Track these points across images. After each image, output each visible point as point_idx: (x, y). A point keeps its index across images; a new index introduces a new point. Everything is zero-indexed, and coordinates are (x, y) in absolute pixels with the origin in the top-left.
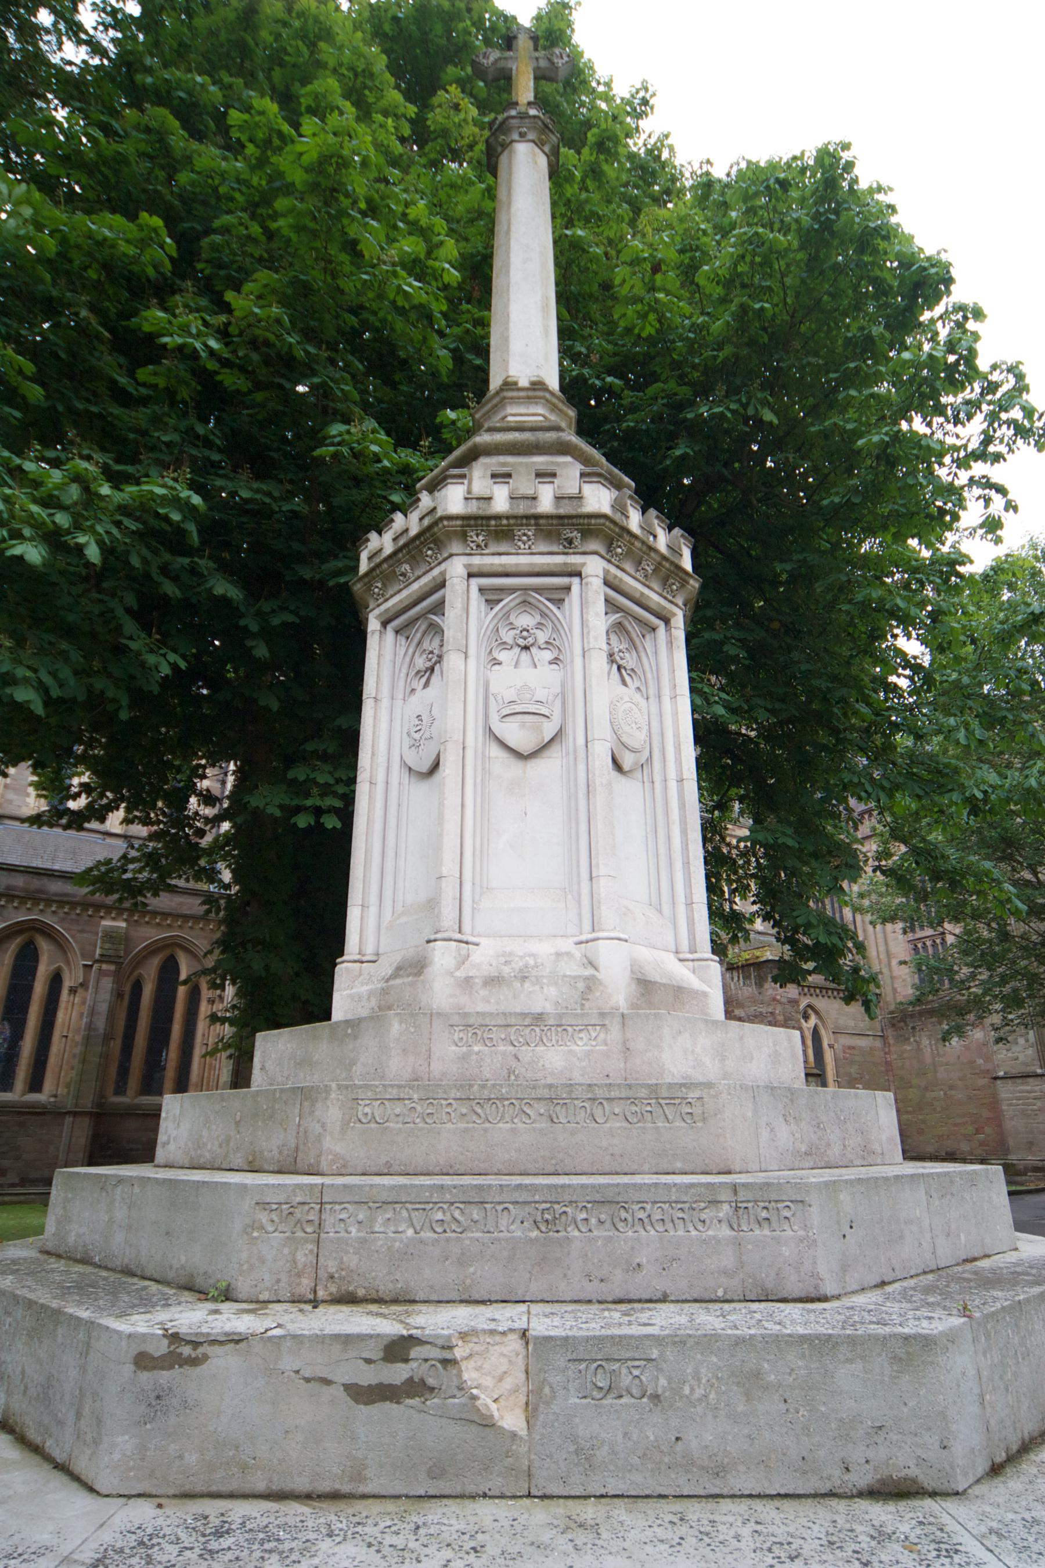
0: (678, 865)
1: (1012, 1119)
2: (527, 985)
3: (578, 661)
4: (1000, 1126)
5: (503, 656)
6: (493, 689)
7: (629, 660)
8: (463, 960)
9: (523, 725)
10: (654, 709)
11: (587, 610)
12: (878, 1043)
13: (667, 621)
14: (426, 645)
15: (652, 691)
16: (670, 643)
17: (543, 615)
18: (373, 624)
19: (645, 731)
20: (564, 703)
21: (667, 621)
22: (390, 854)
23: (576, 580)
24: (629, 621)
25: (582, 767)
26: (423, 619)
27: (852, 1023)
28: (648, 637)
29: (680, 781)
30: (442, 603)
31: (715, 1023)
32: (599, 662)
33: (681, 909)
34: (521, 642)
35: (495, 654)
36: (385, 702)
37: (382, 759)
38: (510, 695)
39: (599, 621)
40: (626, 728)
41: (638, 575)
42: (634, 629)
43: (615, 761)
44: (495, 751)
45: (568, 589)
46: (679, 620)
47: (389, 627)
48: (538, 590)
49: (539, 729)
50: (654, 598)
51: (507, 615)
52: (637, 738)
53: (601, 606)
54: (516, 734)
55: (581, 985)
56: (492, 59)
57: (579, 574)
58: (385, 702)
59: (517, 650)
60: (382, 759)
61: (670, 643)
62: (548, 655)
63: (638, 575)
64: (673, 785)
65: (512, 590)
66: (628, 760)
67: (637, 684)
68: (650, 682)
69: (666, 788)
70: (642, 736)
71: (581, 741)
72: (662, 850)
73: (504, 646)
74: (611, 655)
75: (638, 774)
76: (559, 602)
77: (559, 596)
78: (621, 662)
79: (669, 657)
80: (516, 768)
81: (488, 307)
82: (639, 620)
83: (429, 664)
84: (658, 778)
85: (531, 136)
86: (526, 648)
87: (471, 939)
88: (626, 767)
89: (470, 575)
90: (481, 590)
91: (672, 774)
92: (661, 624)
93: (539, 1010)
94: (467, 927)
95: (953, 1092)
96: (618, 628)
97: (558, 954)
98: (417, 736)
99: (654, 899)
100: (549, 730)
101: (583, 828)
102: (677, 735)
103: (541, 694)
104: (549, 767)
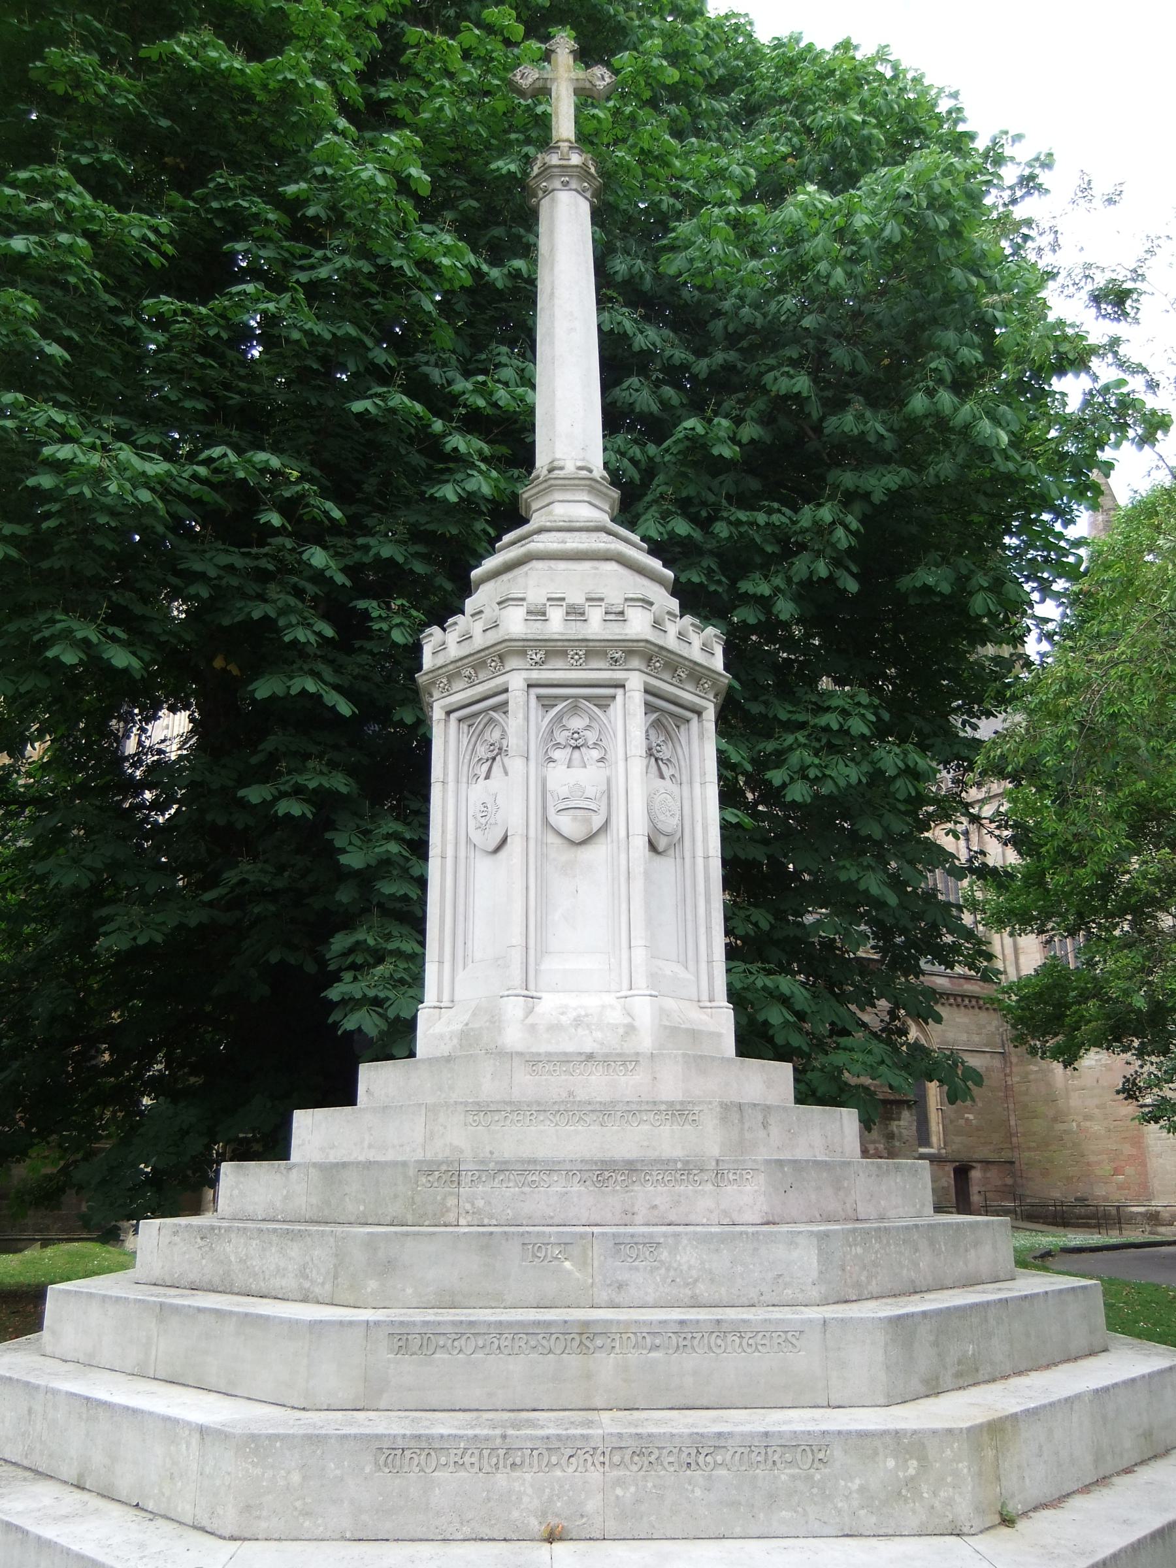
0: (702, 930)
1: (1159, 1156)
2: (580, 1030)
3: (621, 764)
4: (1144, 1164)
5: (557, 754)
6: (550, 785)
7: (666, 752)
8: (530, 1011)
9: (575, 819)
10: (686, 794)
11: (628, 718)
12: (997, 1062)
13: (699, 714)
14: (487, 736)
15: (685, 778)
16: (701, 736)
17: (591, 718)
18: (437, 714)
19: (678, 816)
20: (609, 798)
21: (699, 714)
22: (461, 918)
23: (620, 691)
24: (665, 716)
25: (623, 856)
26: (484, 713)
27: (964, 1037)
28: (682, 728)
29: (706, 858)
30: (506, 703)
31: (728, 1060)
32: (638, 764)
33: (703, 966)
34: (572, 742)
35: (551, 754)
36: (451, 785)
37: (450, 837)
38: (564, 792)
39: (638, 722)
40: (662, 817)
41: (674, 681)
42: (670, 723)
43: (650, 843)
44: (552, 839)
45: (614, 697)
46: (710, 714)
47: (453, 716)
48: (587, 698)
49: (588, 821)
50: (687, 696)
51: (561, 718)
52: (669, 823)
53: (641, 709)
54: (567, 824)
55: (621, 1031)
56: (530, 80)
57: (623, 686)
58: (451, 785)
59: (569, 750)
60: (450, 837)
61: (701, 736)
62: (596, 754)
63: (674, 681)
64: (700, 861)
65: (566, 698)
66: (662, 843)
67: (672, 771)
68: (683, 771)
69: (694, 864)
70: (675, 821)
71: (623, 834)
72: (690, 917)
73: (558, 745)
74: (650, 749)
75: (671, 852)
76: (604, 707)
77: (604, 703)
78: (658, 755)
79: (702, 747)
80: (569, 854)
81: (534, 361)
82: (672, 714)
83: (490, 755)
84: (687, 855)
85: (574, 184)
86: (577, 747)
87: (534, 994)
88: (660, 849)
89: (529, 686)
90: (538, 697)
91: (700, 853)
92: (695, 717)
93: (589, 1050)
94: (532, 986)
95: (1088, 1124)
96: (657, 725)
97: (603, 1007)
98: (483, 821)
99: (682, 958)
100: (597, 822)
101: (624, 906)
102: (704, 818)
103: (591, 792)
104: (597, 853)
